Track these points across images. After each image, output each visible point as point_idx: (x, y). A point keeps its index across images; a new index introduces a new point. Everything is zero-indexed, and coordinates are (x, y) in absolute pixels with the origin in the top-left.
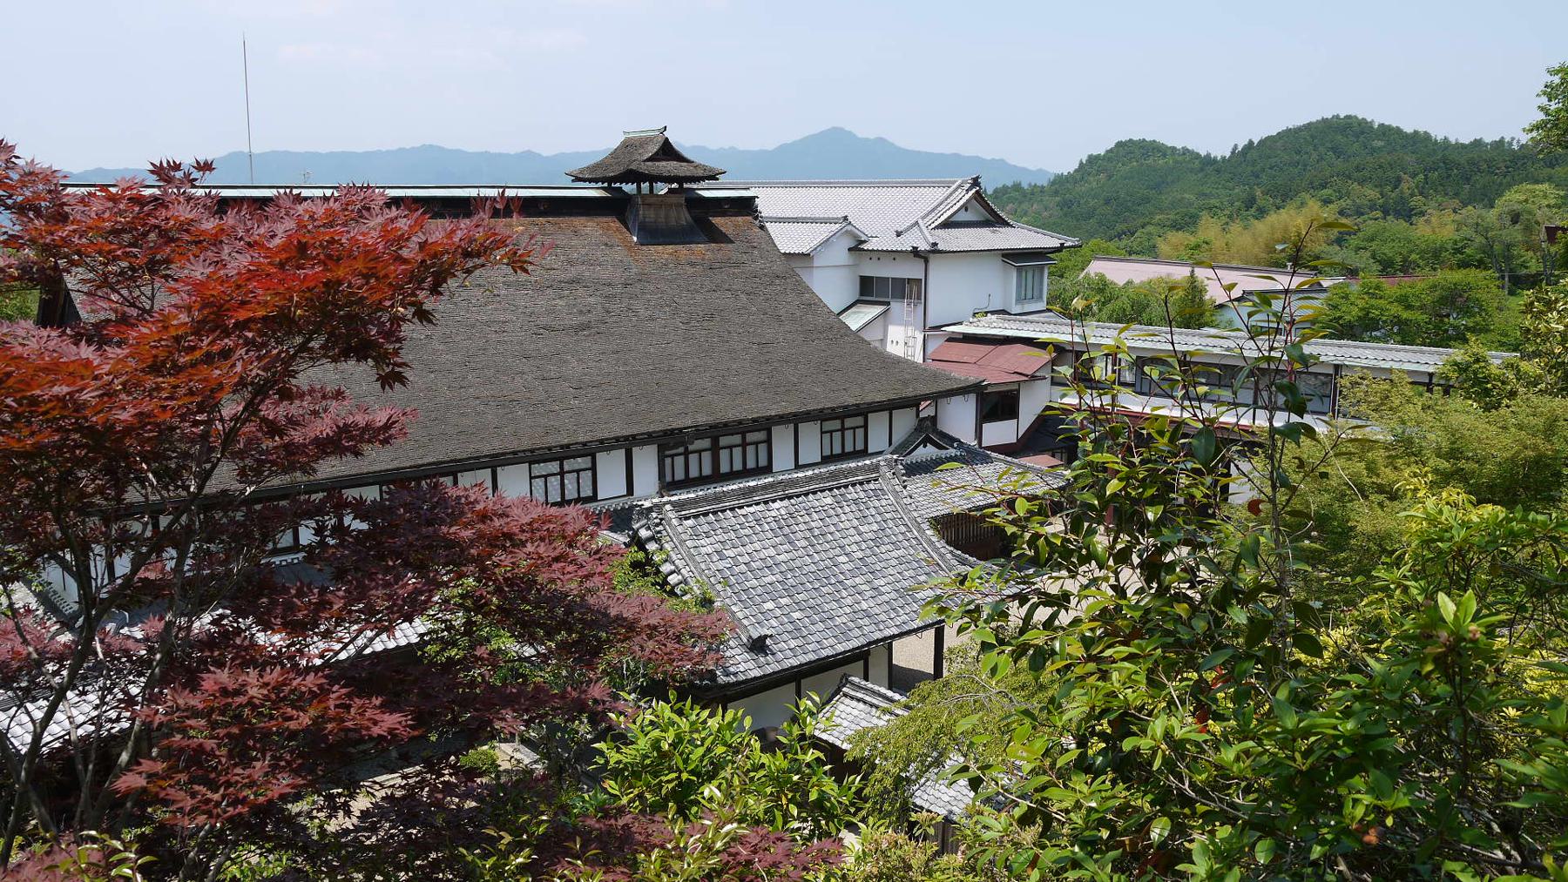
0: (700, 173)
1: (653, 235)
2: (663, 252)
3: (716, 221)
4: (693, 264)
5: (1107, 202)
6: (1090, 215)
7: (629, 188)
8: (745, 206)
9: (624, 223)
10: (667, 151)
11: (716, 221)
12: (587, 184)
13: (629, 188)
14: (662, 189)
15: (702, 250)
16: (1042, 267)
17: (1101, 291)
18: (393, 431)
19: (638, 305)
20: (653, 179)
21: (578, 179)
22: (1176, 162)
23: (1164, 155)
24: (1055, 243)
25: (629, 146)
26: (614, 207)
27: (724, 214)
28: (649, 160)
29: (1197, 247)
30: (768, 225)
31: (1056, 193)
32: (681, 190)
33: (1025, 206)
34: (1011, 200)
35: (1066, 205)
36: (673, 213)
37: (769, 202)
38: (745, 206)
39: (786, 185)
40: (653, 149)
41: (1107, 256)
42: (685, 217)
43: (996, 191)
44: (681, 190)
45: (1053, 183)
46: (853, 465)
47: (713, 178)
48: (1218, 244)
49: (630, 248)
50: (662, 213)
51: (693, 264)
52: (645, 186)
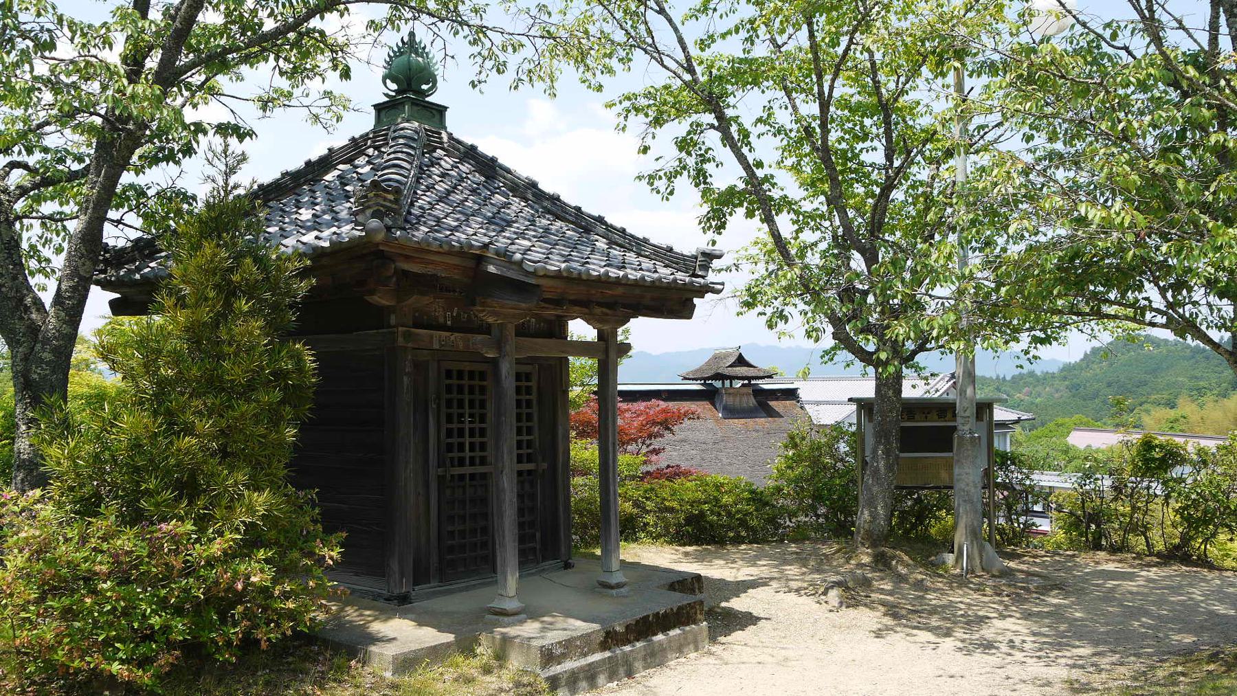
0: (762, 374)
1: (732, 412)
2: (738, 423)
3: (771, 403)
4: (757, 431)
5: (1109, 385)
6: (1096, 395)
7: (718, 384)
8: (791, 394)
9: (713, 404)
10: (741, 361)
11: (771, 403)
12: (607, 418)
13: (718, 384)
14: (738, 384)
15: (762, 422)
16: (1005, 434)
17: (1066, 452)
18: (988, 669)
19: (721, 455)
20: (732, 378)
21: (685, 379)
22: (1169, 351)
23: (1158, 346)
24: (1014, 417)
25: (717, 358)
26: (708, 395)
27: (777, 399)
28: (731, 366)
29: (1176, 420)
30: (807, 407)
31: (1065, 378)
32: (749, 385)
33: (1039, 389)
34: (1026, 384)
35: (1075, 388)
36: (745, 399)
37: (806, 391)
38: (791, 394)
39: (824, 380)
40: (732, 360)
41: (1079, 426)
42: (752, 401)
43: (1013, 377)
44: (749, 385)
45: (1063, 370)
46: (561, 509)
47: (770, 377)
48: (1194, 418)
49: (717, 420)
50: (738, 399)
51: (757, 431)
52: (727, 383)
